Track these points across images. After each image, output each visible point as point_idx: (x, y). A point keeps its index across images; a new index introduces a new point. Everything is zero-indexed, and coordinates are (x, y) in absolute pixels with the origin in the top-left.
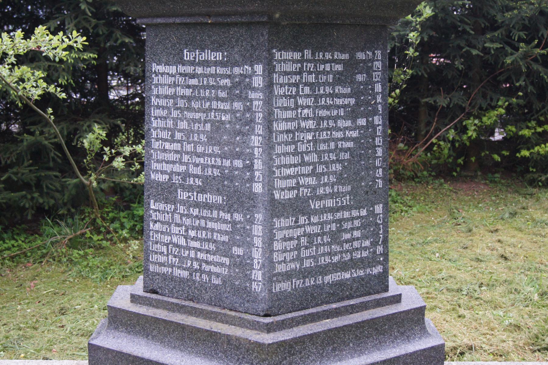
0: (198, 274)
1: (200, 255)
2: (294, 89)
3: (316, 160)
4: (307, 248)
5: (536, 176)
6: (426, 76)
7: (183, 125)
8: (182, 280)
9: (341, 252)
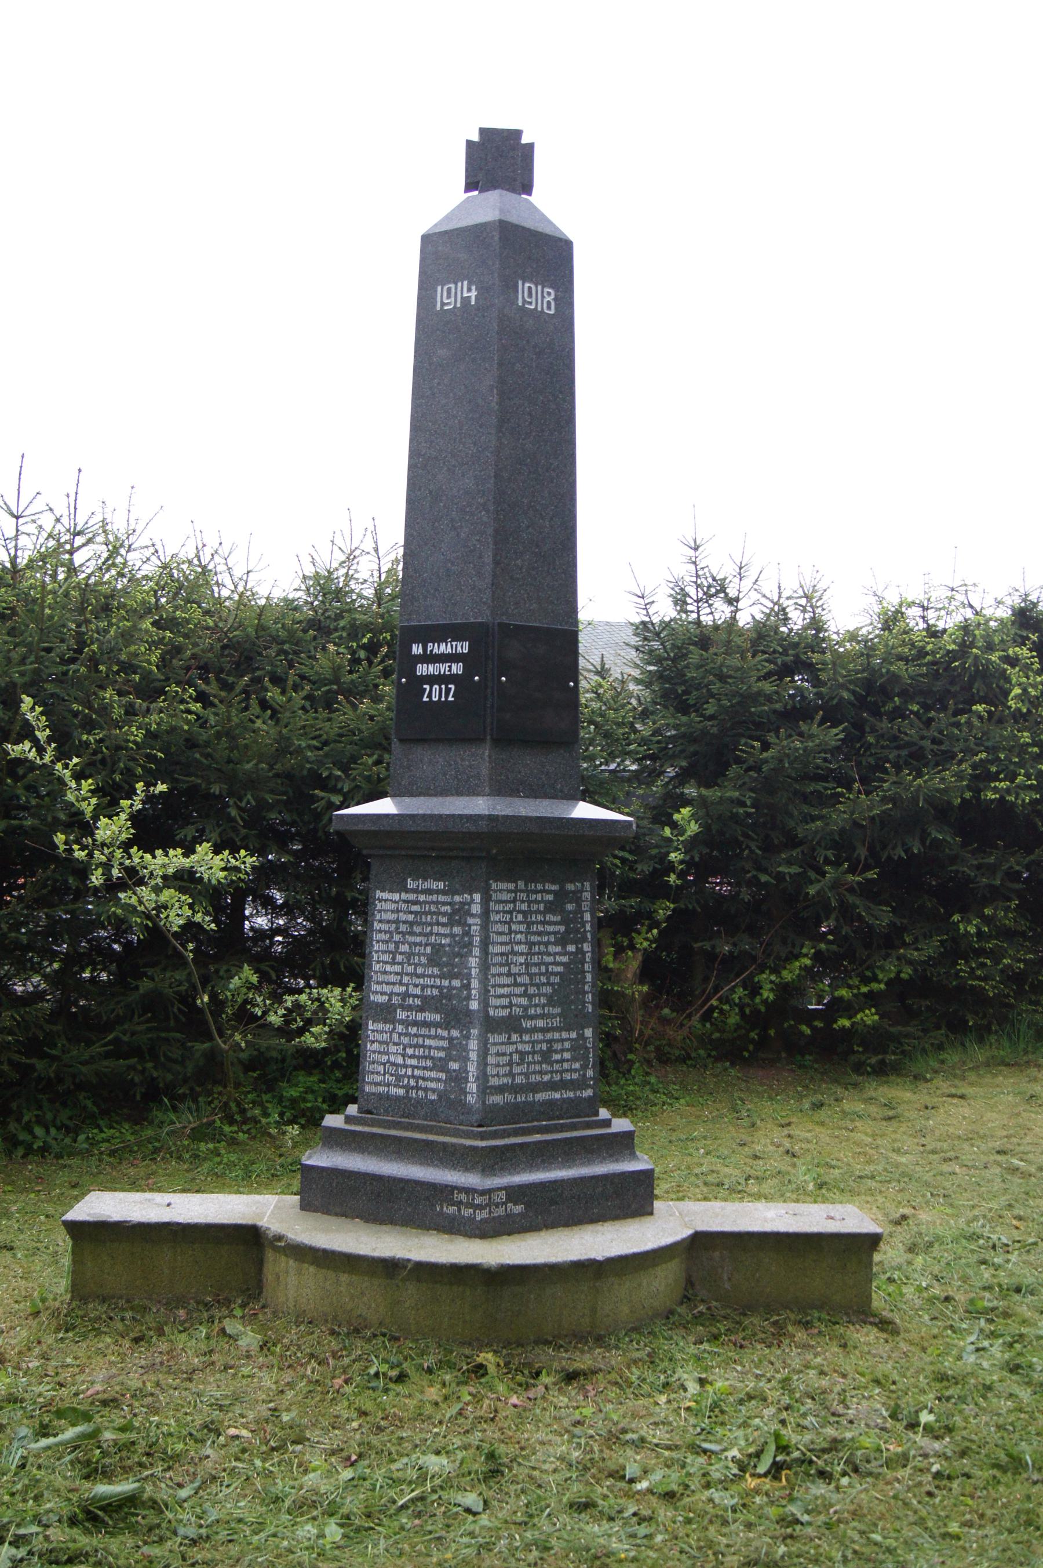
0: (414, 1091)
1: (417, 1072)
2: (509, 916)
3: (528, 982)
4: (518, 1064)
5: (863, 1058)
6: (699, 910)
7: (404, 948)
8: (397, 1098)
9: (552, 1072)
